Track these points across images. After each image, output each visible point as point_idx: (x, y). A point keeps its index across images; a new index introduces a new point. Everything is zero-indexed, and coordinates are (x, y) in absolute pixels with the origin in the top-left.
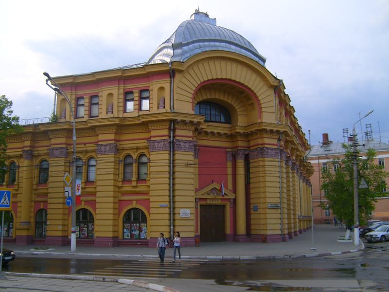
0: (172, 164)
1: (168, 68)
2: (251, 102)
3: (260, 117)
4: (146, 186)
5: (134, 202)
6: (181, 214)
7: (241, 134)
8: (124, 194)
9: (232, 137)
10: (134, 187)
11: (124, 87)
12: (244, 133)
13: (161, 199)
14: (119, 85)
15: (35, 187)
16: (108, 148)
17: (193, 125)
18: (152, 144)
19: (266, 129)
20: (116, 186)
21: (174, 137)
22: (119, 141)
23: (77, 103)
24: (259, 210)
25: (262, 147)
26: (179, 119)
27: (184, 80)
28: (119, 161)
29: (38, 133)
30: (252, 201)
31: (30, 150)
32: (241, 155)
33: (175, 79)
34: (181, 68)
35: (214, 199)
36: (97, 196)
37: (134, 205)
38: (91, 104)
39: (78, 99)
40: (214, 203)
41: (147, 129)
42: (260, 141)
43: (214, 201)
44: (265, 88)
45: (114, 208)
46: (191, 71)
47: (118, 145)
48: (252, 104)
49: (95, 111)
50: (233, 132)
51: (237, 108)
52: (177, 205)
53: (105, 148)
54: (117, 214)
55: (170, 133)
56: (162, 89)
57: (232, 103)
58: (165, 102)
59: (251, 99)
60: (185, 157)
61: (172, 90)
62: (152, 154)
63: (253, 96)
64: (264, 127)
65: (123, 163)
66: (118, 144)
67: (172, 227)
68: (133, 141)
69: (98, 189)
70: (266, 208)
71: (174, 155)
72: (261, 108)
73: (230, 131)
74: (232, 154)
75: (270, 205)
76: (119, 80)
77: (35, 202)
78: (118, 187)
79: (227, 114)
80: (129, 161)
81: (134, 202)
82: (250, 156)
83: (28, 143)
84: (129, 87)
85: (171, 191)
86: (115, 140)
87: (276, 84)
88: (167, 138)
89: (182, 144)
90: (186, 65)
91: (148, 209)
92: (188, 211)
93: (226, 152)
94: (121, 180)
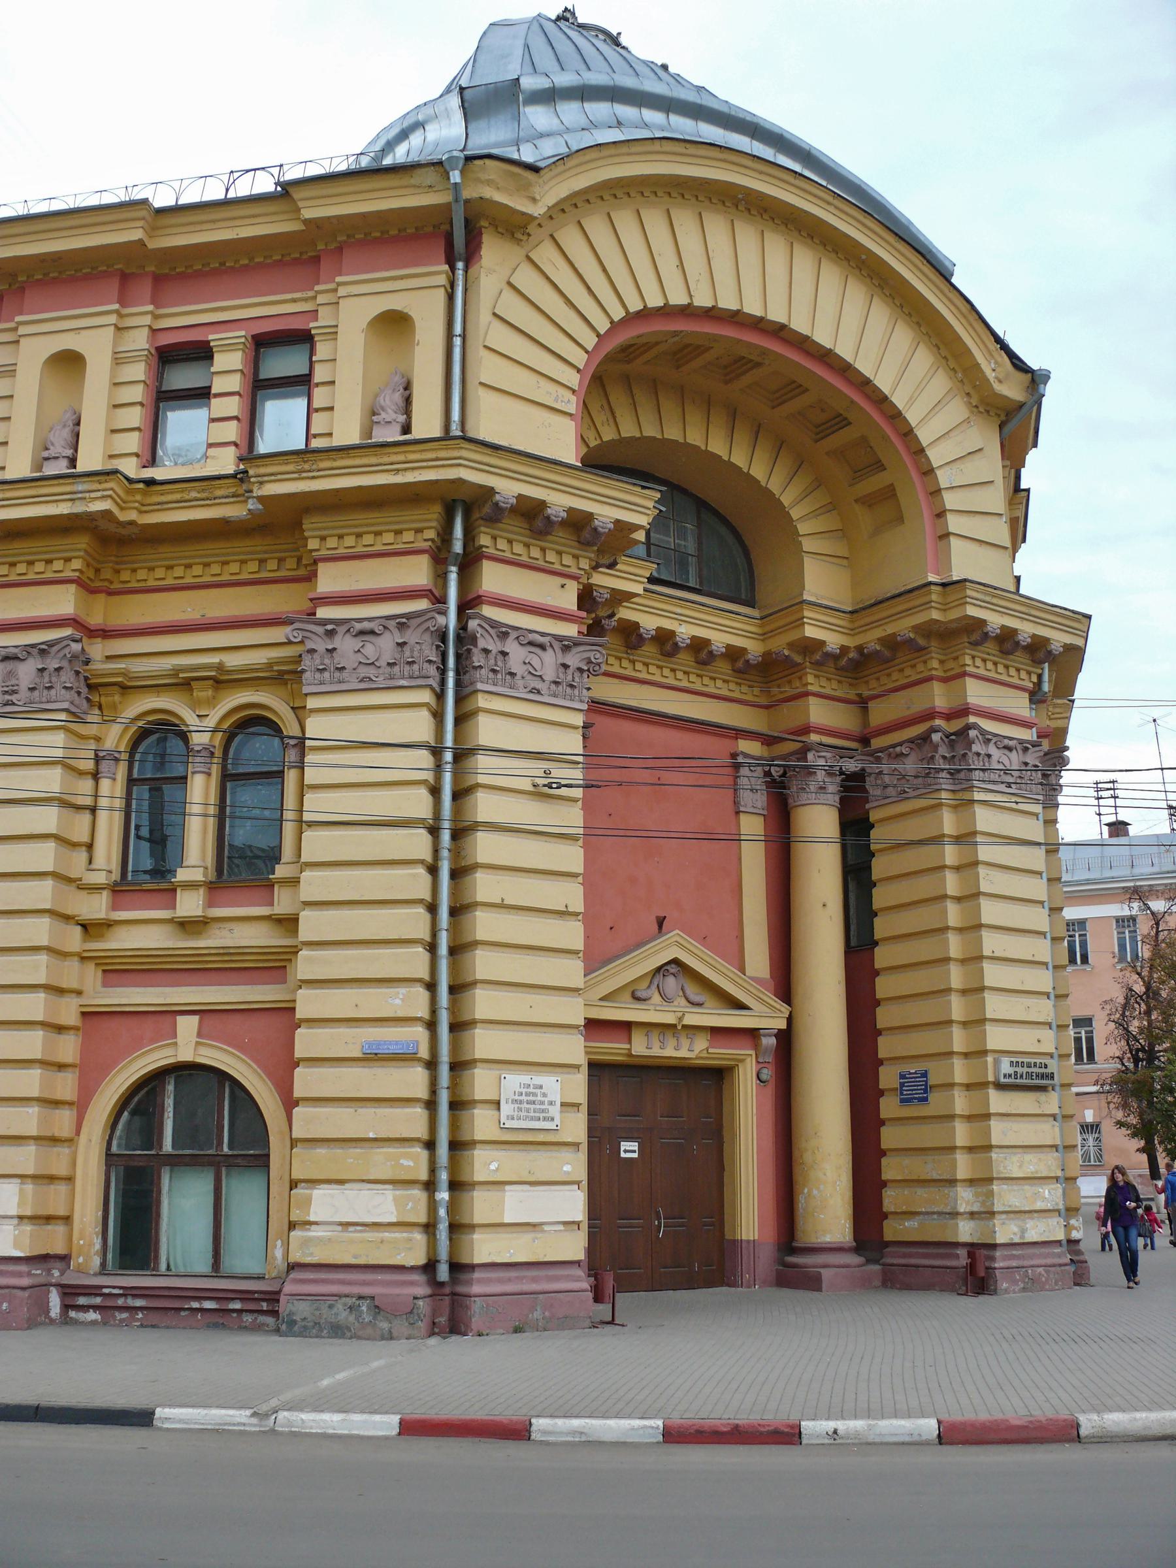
0: (454, 759)
3: (943, 559)
4: (268, 918)
5: (187, 1026)
6: (506, 1109)
7: (828, 655)
8: (117, 970)
9: (769, 675)
10: (187, 926)
12: (844, 649)
14: (123, 302)
17: (585, 544)
18: (321, 645)
19: (983, 623)
20: (67, 918)
21: (466, 606)
24: (933, 1097)
26: (508, 489)
27: (526, 279)
28: (97, 759)
30: (886, 1047)
35: (673, 1026)
37: (186, 1044)
40: (669, 1052)
41: (291, 563)
43: (685, 1042)
44: (957, 410)
46: (571, 239)
48: (889, 494)
50: (779, 644)
51: (795, 514)
52: (483, 1043)
55: (441, 577)
56: (394, 325)
57: (774, 486)
58: (408, 401)
60: (526, 733)
61: (458, 329)
62: (313, 711)
63: (889, 431)
64: (972, 611)
65: (122, 771)
67: (443, 1195)
71: (461, 720)
74: (768, 774)
75: (1006, 1067)
76: (125, 278)
78: (85, 926)
81: (187, 1026)
82: (869, 782)
84: (185, 316)
85: (443, 950)
87: (1012, 389)
88: (422, 604)
89: (517, 654)
92: (552, 1086)
93: (734, 756)
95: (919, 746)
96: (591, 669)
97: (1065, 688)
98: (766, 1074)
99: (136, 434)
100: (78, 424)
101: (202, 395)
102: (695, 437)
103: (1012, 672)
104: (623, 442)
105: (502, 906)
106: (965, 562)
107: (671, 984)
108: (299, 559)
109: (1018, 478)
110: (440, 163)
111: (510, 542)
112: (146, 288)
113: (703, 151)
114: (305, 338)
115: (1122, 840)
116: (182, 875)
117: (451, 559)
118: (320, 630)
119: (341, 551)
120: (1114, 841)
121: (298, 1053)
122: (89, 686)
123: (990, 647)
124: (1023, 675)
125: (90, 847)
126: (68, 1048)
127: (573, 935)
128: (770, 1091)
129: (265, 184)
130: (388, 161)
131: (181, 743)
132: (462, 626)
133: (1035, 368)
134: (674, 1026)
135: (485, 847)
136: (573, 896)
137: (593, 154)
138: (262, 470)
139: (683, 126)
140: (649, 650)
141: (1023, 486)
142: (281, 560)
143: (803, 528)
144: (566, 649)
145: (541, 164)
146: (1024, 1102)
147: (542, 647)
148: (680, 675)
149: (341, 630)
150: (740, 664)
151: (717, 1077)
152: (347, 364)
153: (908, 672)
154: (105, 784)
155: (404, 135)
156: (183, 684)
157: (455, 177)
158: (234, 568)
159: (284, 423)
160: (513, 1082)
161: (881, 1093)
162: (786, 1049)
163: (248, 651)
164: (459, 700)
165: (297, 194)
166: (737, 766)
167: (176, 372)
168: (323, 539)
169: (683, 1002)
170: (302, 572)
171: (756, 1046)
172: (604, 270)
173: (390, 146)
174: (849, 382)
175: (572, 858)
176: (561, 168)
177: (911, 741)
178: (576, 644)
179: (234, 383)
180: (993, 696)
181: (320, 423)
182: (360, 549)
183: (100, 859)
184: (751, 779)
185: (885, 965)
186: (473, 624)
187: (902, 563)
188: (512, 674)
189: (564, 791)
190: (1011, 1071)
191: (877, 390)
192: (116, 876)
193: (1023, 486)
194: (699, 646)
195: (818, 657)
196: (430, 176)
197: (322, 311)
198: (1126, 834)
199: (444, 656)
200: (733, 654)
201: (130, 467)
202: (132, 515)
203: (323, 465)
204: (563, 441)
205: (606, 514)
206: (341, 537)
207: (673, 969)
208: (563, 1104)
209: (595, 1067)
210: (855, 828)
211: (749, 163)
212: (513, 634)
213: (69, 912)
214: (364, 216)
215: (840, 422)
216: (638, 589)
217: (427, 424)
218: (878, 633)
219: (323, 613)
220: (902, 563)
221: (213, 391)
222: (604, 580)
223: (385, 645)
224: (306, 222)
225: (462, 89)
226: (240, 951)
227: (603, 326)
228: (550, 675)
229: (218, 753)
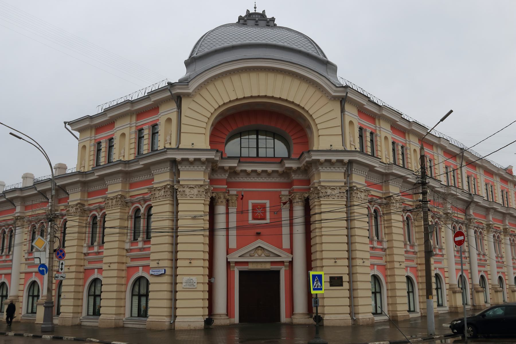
5: (141, 268)
27: (193, 105)
32: (297, 200)
54: (125, 284)
81: (141, 268)
107: (260, 252)
126: (124, 274)
160: (186, 278)
223: (337, 191)
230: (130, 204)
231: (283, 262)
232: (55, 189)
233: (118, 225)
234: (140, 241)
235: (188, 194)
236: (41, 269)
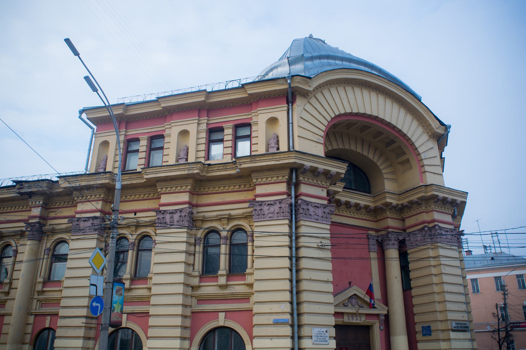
1: (285, 87)
2: (404, 158)
5: (222, 315)
7: (393, 206)
8: (202, 300)
9: (376, 213)
10: (221, 287)
11: (208, 120)
12: (398, 205)
13: (276, 308)
14: (199, 116)
15: (39, 287)
16: (176, 217)
17: (328, 178)
18: (258, 208)
19: (437, 196)
21: (296, 197)
22: (197, 206)
23: (127, 148)
25: (431, 225)
26: (308, 164)
27: (308, 107)
29: (59, 195)
30: (417, 319)
31: (39, 223)
33: (295, 106)
34: (306, 88)
36: (151, 303)
37: (221, 321)
38: (151, 149)
39: (130, 141)
40: (354, 321)
41: (248, 186)
42: (425, 217)
43: (355, 318)
44: (425, 137)
45: (183, 327)
47: (195, 212)
48: (408, 161)
49: (157, 159)
50: (379, 204)
51: (381, 167)
53: (172, 217)
55: (289, 188)
56: (273, 121)
57: (375, 160)
58: (278, 141)
59: (404, 153)
60: (315, 232)
61: (291, 122)
63: (407, 144)
66: (195, 210)
68: (223, 206)
69: (155, 290)
70: (449, 330)
71: (297, 228)
72: (423, 166)
73: (374, 202)
74: (377, 240)
75: (454, 324)
77: (36, 315)
79: (360, 177)
80: (213, 238)
81: (222, 315)
83: (36, 212)
84: (216, 120)
85: (294, 293)
86: (41, 217)
87: (441, 131)
88: (285, 196)
89: (312, 209)
90: (315, 84)
91: (250, 328)
94: (197, 274)
95: (421, 231)
96: (331, 213)
97: (461, 214)
98: (382, 328)
99: (204, 152)
100: (188, 149)
101: (221, 141)
102: (353, 148)
103: (446, 209)
104: (333, 150)
105: (310, 280)
106: (430, 179)
107: (354, 301)
108: (250, 185)
109: (441, 155)
110: (285, 78)
111: (308, 179)
112: (205, 113)
113: (354, 71)
114: (249, 125)
115: (471, 256)
116: (220, 272)
117: (292, 183)
118: (257, 204)
119: (262, 182)
120: (468, 256)
121: (254, 323)
122: (193, 220)
123: (440, 203)
124: (450, 210)
125: (193, 265)
126: (188, 323)
127: (330, 288)
128: (383, 332)
129: (236, 85)
130: (267, 78)
131: (218, 236)
132: (296, 202)
133: (446, 124)
134: (355, 313)
135: (304, 263)
136: (329, 277)
137: (325, 73)
138: (241, 161)
139: (346, 64)
140: (343, 207)
141: (443, 157)
142: (245, 185)
143: (384, 171)
144: (325, 207)
145: (312, 77)
146: (461, 335)
147: (318, 207)
148: (352, 213)
149: (263, 204)
150: (368, 210)
151: (368, 328)
152: (260, 131)
153: (416, 210)
154: (197, 247)
155: (272, 70)
156: (219, 219)
157: (289, 81)
158: (232, 187)
159: (244, 148)
161: (416, 333)
162: (387, 320)
163: (238, 210)
164: (296, 222)
165: (246, 87)
166: (368, 238)
167: (214, 134)
168: (257, 179)
169: (358, 306)
170: (251, 188)
171: (379, 319)
172: (329, 104)
173: (267, 74)
174: (395, 131)
175: (329, 266)
176: (317, 77)
177: (419, 230)
178: (327, 206)
179: (230, 137)
180: (442, 217)
181: (254, 148)
182: (267, 182)
183: (196, 267)
184: (373, 242)
185: (304, 278)
186: (299, 202)
187: (412, 179)
188: (311, 215)
189: (326, 247)
190: (456, 326)
191: (403, 133)
192: (201, 273)
193: (443, 157)
194: (357, 205)
195: (390, 207)
196: (282, 81)
197: (254, 118)
198: (471, 254)
199: (291, 210)
200: (366, 207)
201: (202, 160)
202: (205, 174)
203: (257, 159)
204: (320, 151)
205: (334, 170)
206: (262, 179)
207: (354, 297)
208: (330, 337)
209: (336, 326)
210: (403, 256)
211: (365, 73)
212: (310, 204)
213: (188, 283)
214: (264, 92)
215: (393, 142)
216: (341, 190)
217: (284, 147)
218: (407, 200)
219: (258, 199)
220: (412, 179)
221: (225, 140)
222: (333, 188)
223: (276, 208)
224: (249, 94)
225: (288, 58)
226: (237, 294)
227: (329, 119)
228: (320, 215)
229: (229, 238)
230: (199, 224)
231: (378, 315)
232: (46, 196)
233: (185, 249)
234: (222, 275)
235: (266, 212)
236: (94, 304)
